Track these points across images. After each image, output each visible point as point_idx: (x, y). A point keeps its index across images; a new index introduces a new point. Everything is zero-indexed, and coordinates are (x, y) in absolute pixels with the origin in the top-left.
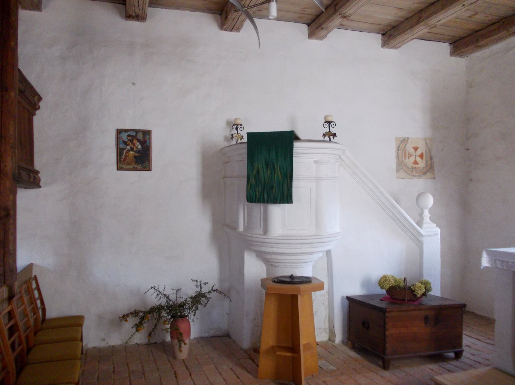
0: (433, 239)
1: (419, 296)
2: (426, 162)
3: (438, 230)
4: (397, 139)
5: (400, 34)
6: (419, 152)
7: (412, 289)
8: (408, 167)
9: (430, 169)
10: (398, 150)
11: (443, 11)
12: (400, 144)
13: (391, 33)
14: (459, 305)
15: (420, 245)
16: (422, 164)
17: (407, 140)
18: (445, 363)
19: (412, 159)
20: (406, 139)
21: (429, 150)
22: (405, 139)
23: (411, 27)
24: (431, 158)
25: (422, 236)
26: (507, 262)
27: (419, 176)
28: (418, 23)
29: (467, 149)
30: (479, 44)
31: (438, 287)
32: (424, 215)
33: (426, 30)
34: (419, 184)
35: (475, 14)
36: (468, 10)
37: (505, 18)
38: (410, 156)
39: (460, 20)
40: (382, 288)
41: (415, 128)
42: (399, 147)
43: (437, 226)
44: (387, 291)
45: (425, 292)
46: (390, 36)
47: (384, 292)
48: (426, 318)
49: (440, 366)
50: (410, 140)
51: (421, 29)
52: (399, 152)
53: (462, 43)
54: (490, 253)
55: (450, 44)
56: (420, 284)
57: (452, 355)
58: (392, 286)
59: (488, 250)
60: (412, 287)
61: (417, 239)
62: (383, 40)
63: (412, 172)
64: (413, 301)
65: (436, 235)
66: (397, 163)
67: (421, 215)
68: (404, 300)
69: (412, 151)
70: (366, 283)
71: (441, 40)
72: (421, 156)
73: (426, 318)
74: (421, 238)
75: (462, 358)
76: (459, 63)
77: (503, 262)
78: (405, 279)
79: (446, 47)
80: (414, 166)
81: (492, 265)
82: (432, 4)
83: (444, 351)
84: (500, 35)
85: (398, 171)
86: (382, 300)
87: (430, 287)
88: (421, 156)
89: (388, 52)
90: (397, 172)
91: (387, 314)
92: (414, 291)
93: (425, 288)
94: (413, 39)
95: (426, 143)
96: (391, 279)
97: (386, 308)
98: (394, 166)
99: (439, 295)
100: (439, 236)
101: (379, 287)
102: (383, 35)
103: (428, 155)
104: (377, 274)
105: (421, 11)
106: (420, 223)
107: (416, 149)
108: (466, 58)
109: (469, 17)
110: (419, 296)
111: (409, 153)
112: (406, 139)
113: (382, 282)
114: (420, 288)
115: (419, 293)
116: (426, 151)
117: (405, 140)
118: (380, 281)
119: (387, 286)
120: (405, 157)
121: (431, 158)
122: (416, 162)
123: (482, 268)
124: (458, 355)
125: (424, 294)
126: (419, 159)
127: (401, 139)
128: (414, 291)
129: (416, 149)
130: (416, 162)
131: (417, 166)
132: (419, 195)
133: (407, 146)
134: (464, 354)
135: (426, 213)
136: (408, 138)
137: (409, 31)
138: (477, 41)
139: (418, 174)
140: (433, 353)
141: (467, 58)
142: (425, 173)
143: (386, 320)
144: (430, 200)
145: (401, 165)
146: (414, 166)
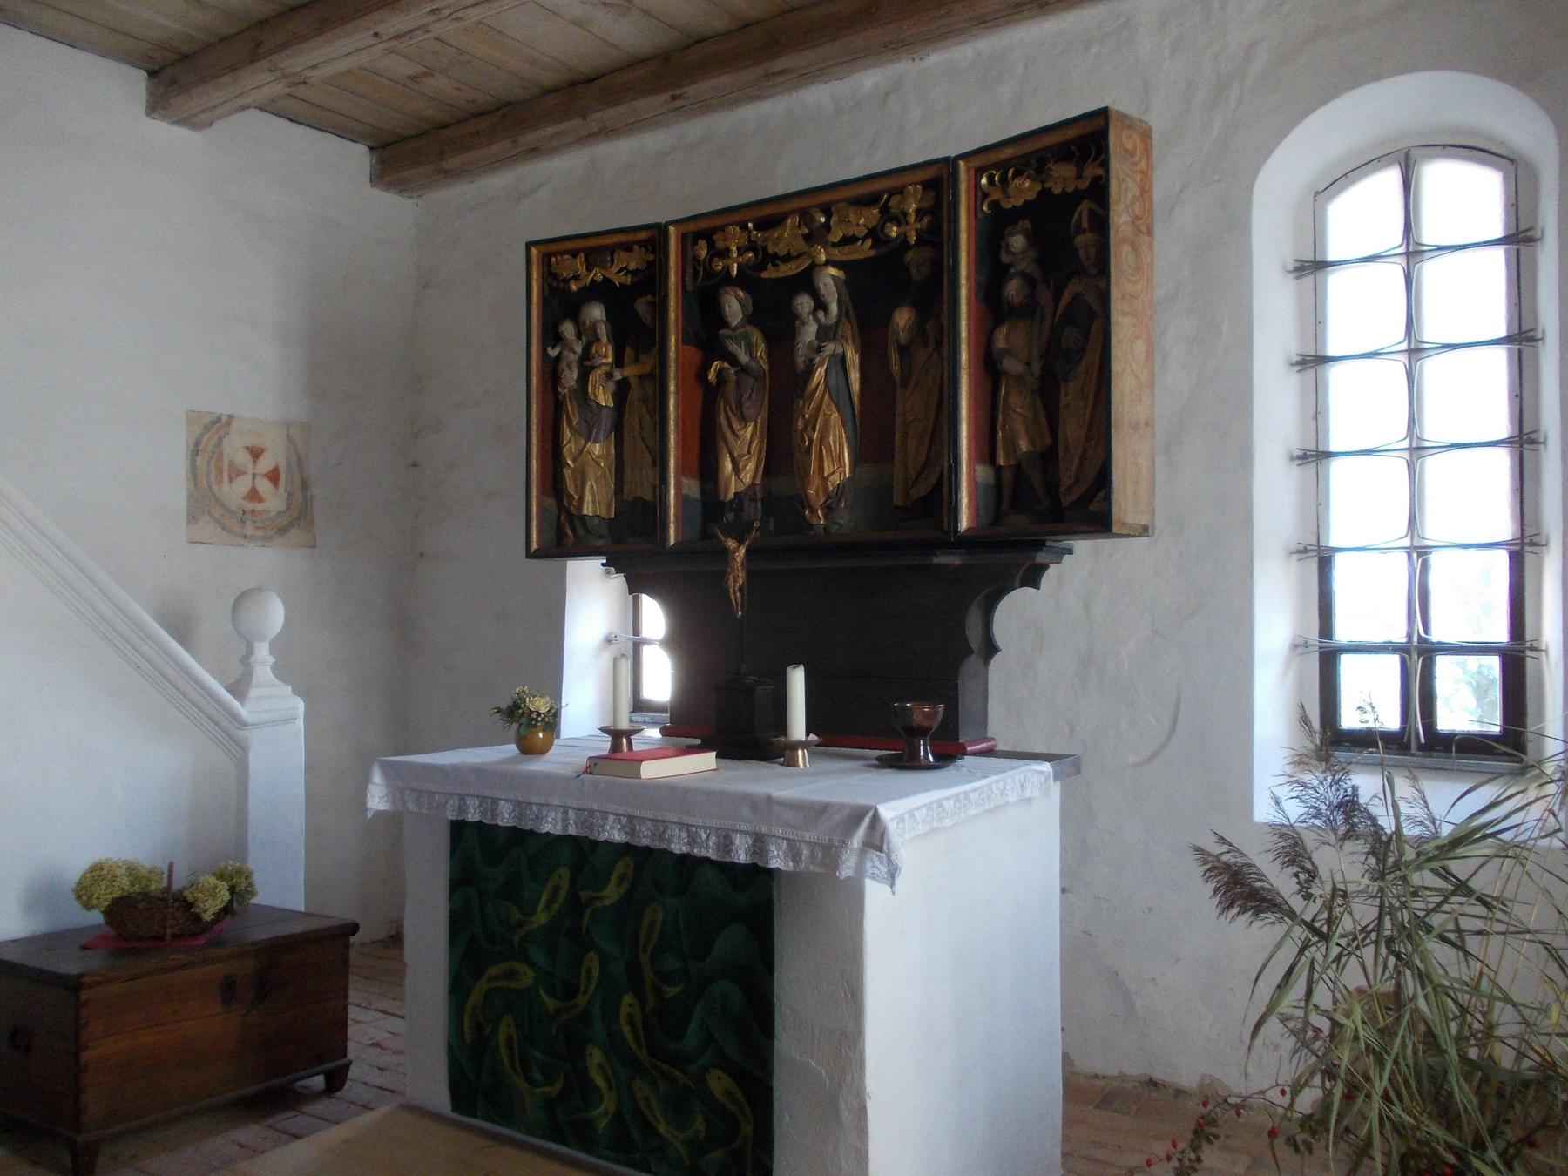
0: (279, 729)
1: (208, 917)
2: (290, 495)
3: (300, 705)
4: (192, 417)
5: (203, 81)
6: (266, 464)
7: (185, 900)
8: (228, 510)
9: (299, 518)
10: (196, 450)
11: (321, 39)
12: (202, 435)
13: (178, 74)
14: (339, 927)
15: (239, 752)
16: (274, 500)
17: (228, 424)
18: (291, 1114)
19: (243, 485)
20: (224, 419)
21: (299, 459)
22: (219, 420)
23: (233, 69)
24: (305, 485)
25: (242, 724)
26: (431, 794)
27: (265, 538)
28: (253, 59)
29: (414, 465)
30: (446, 165)
31: (283, 886)
32: (252, 660)
33: (279, 88)
34: (265, 560)
35: (425, 75)
36: (392, 51)
37: (507, 104)
38: (236, 473)
39: (386, 82)
40: (88, 906)
41: (256, 388)
42: (197, 444)
43: (296, 692)
44: (109, 913)
45: (231, 901)
46: (173, 82)
47: (96, 917)
48: (228, 989)
49: (270, 1127)
50: (235, 425)
51: (262, 81)
52: (199, 460)
53: (410, 150)
54: (391, 771)
55: (371, 149)
56: (213, 880)
57: (318, 1081)
58: (122, 898)
59: (389, 763)
60: (186, 893)
61: (231, 738)
62: (151, 94)
63: (242, 523)
64: (194, 935)
65: (289, 720)
66: (190, 496)
67: (246, 660)
68: (161, 938)
69: (243, 458)
70: (40, 896)
71: (346, 133)
72: (274, 476)
73: (228, 989)
74: (240, 733)
75: (348, 1083)
76: (394, 211)
77: (421, 793)
78: (171, 865)
79: (358, 156)
80: (249, 506)
81: (393, 803)
82: (293, 9)
83: (290, 1077)
84: (495, 148)
85: (192, 518)
86: (84, 948)
87: (250, 885)
88: (274, 476)
89: (162, 131)
90: (189, 522)
91: (84, 996)
92: (191, 905)
93: (232, 890)
94: (244, 108)
95: (289, 437)
96: (118, 872)
97: (81, 976)
98: (178, 499)
99: (297, 902)
100: (300, 724)
101: (77, 905)
102: (152, 74)
103: (297, 479)
104: (76, 865)
105: (262, 23)
106: (239, 688)
107: (256, 453)
108: (415, 201)
109: (413, 78)
110: (208, 917)
111: (231, 464)
112: (224, 419)
113: (84, 892)
114: (213, 892)
115: (209, 909)
116: (288, 461)
117: (219, 425)
118: (79, 883)
119: (105, 895)
120: (220, 472)
121: (305, 485)
122: (254, 495)
123: (370, 815)
124: (336, 1080)
125: (226, 910)
126: (264, 486)
127: (207, 420)
128: (191, 905)
129: (256, 453)
130: (254, 495)
131: (258, 507)
132: (237, 600)
133: (225, 442)
134: (353, 1073)
135: (263, 652)
136: (230, 417)
137: (227, 79)
138: (441, 155)
139: (260, 533)
140: (232, 1095)
141: (420, 202)
142: (283, 531)
143: (84, 1012)
144: (275, 615)
145: (203, 502)
146: (249, 506)
